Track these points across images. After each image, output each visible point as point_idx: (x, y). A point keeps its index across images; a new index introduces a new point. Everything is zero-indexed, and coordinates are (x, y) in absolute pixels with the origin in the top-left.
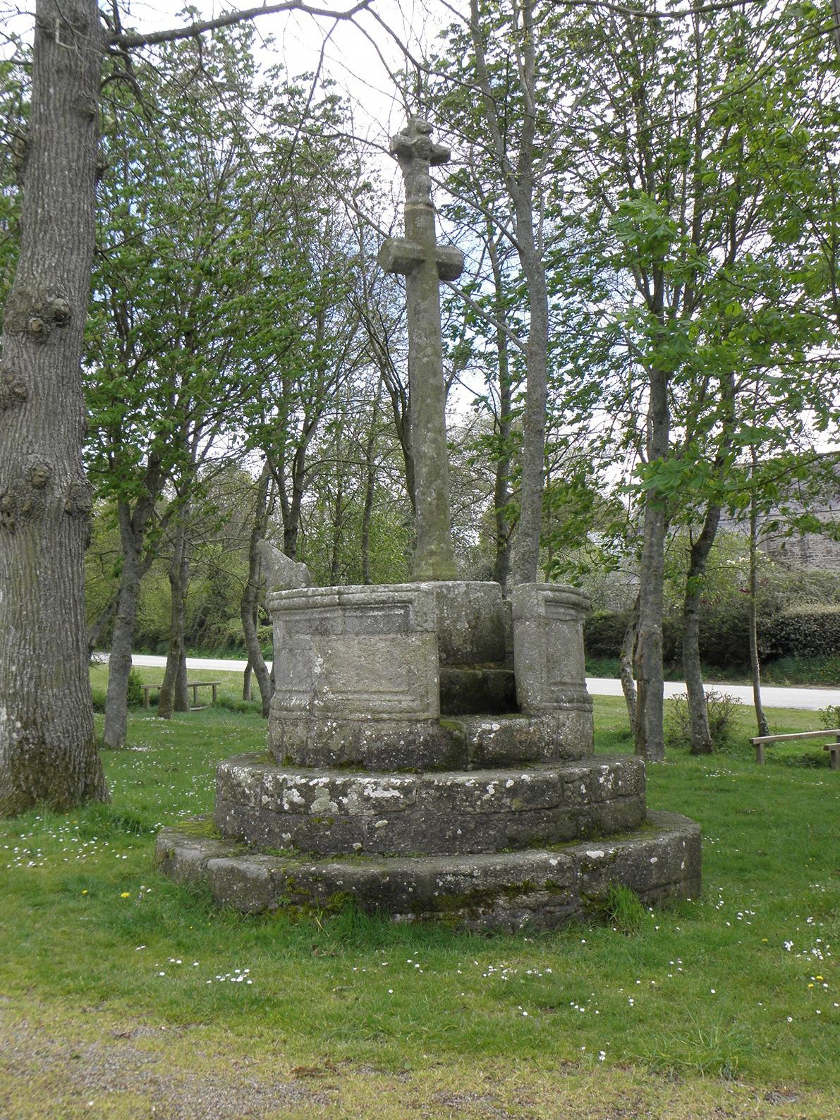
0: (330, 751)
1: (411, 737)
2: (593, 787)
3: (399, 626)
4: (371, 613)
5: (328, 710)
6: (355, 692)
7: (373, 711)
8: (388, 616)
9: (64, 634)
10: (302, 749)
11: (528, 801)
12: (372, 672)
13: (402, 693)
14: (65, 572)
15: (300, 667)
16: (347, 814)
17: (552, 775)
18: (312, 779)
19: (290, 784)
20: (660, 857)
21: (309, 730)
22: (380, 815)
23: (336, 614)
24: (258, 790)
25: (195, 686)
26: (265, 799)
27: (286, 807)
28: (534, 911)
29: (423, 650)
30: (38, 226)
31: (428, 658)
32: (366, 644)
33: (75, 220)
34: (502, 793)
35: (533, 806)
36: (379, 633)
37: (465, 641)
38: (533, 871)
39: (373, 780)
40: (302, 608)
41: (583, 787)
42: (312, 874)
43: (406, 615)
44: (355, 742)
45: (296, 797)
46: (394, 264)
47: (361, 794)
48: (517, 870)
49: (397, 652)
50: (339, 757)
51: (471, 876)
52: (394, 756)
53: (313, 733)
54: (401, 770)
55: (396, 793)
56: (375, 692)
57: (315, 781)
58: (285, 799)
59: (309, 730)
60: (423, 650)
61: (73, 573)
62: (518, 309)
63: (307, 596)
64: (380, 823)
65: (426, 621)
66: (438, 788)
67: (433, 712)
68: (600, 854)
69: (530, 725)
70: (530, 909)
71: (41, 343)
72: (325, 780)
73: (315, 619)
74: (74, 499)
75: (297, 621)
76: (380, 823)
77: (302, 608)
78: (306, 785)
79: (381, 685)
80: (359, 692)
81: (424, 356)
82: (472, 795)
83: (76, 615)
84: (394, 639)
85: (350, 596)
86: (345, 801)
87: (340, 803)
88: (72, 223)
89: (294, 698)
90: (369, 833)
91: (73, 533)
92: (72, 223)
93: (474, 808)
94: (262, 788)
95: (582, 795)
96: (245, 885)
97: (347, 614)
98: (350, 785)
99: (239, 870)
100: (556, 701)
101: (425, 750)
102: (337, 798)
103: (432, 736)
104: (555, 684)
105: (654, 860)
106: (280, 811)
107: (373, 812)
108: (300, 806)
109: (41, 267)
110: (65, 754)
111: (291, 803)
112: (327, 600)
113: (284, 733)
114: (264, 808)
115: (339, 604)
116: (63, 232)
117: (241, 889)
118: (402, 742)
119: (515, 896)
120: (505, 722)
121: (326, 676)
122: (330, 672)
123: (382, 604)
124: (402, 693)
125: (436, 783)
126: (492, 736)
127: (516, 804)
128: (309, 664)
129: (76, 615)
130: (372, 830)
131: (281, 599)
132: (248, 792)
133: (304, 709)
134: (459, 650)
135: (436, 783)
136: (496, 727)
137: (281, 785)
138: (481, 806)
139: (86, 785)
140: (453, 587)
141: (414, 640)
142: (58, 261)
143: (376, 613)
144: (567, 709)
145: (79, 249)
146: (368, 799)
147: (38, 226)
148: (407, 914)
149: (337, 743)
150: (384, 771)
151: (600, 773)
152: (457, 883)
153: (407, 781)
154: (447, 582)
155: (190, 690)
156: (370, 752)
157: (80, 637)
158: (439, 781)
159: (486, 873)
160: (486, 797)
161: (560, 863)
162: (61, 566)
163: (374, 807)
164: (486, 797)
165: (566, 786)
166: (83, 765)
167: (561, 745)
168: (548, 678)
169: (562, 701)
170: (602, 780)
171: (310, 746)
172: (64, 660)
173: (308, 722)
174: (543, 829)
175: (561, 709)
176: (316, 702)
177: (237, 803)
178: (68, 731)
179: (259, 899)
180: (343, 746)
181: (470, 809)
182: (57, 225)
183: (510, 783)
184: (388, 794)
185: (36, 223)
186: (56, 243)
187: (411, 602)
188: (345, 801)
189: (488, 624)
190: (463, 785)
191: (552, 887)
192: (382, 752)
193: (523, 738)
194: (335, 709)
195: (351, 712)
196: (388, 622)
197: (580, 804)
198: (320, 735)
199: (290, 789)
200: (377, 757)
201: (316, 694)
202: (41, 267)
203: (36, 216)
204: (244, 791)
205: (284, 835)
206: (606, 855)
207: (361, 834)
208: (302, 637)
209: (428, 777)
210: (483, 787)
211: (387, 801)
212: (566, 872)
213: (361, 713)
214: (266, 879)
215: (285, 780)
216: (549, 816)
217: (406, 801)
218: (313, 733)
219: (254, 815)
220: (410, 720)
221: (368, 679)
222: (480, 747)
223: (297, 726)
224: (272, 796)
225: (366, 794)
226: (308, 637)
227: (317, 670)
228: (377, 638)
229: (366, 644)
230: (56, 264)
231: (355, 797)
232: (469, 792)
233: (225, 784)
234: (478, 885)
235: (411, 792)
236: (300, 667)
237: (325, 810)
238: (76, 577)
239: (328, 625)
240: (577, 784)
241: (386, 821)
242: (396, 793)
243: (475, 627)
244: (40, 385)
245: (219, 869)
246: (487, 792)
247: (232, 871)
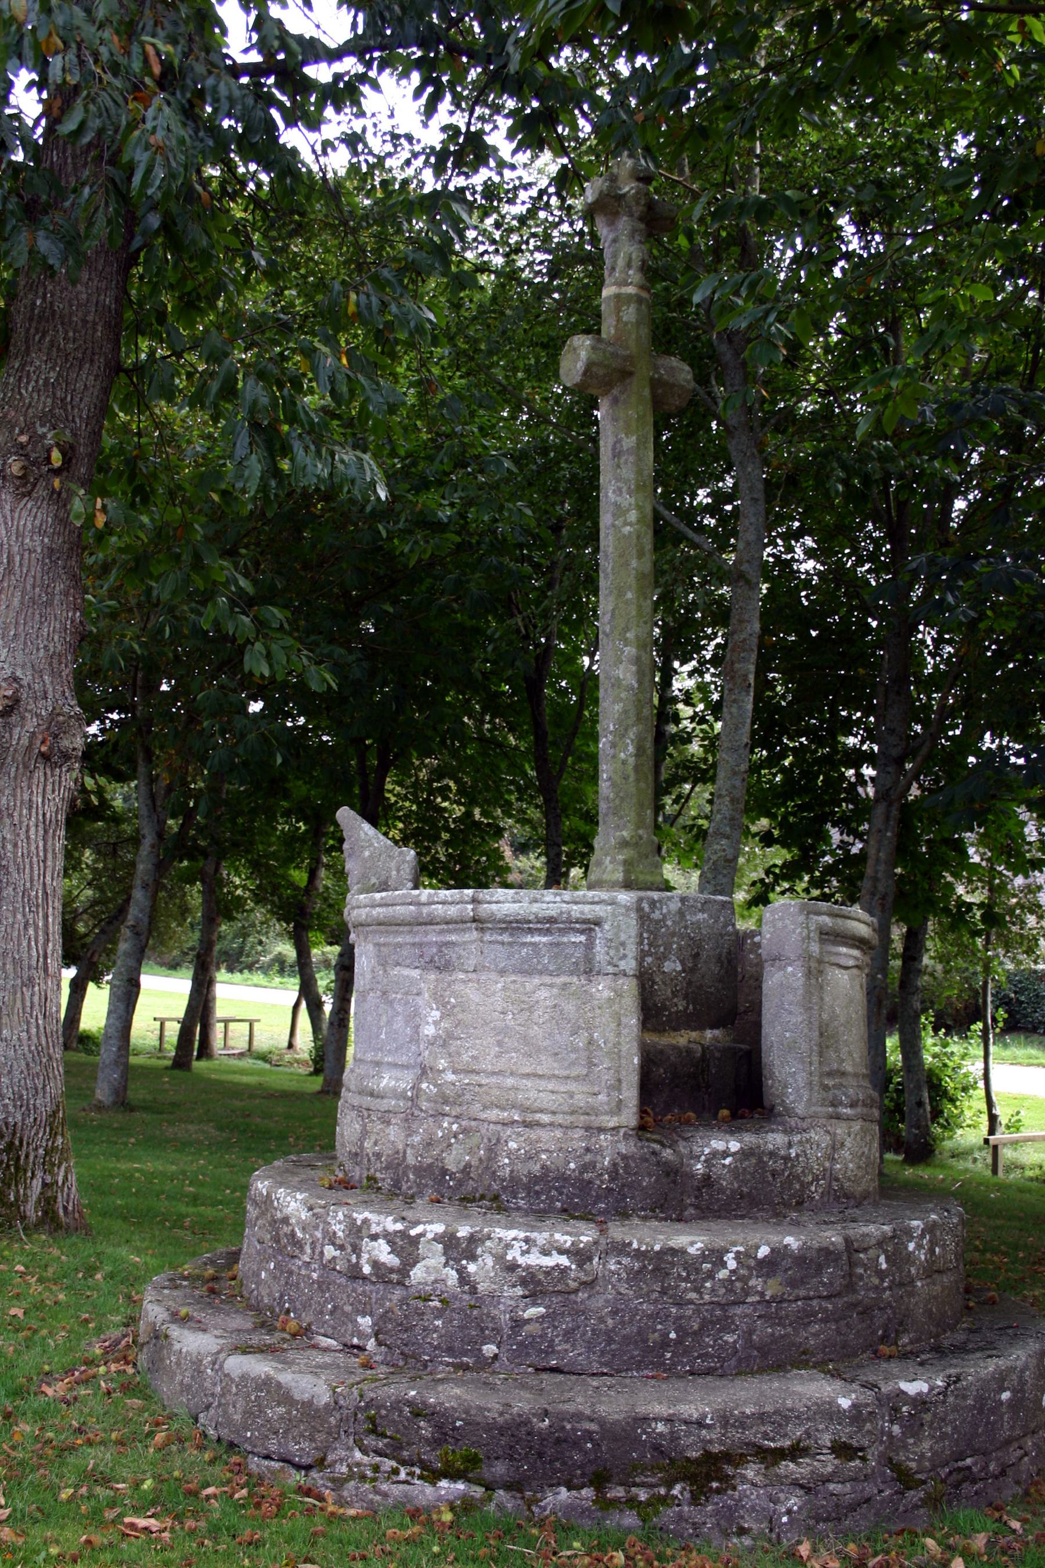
0: (444, 1172)
1: (588, 1157)
2: (899, 1258)
3: (576, 964)
4: (529, 939)
5: (446, 1102)
6: (494, 1073)
7: (525, 1109)
8: (558, 944)
9: (25, 944)
10: (396, 1165)
11: (793, 1284)
12: (525, 1039)
13: (577, 1078)
14: (33, 848)
15: (399, 1023)
16: (473, 1290)
17: (833, 1237)
18: (417, 1223)
19: (375, 1229)
20: (1014, 1391)
21: (410, 1132)
22: (533, 1296)
23: (467, 937)
24: (319, 1234)
25: (226, 1022)
26: (330, 1251)
27: (367, 1269)
28: (807, 1490)
29: (616, 1007)
30: (34, 325)
31: (624, 1020)
32: (515, 992)
33: (90, 318)
34: (749, 1268)
35: (802, 1293)
36: (541, 973)
37: (675, 994)
38: (808, 1419)
39: (522, 1235)
40: (409, 924)
41: (882, 1259)
42: (410, 1403)
43: (590, 945)
44: (489, 1159)
45: (383, 1252)
46: (585, 373)
47: (500, 1258)
48: (781, 1418)
49: (569, 1007)
50: (460, 1183)
51: (700, 1424)
52: (556, 1189)
53: (417, 1139)
54: (569, 1213)
55: (564, 1261)
56: (527, 1076)
57: (419, 1229)
58: (365, 1256)
59: (410, 1132)
60: (616, 1007)
61: (45, 850)
62: (297, 867)
63: (419, 904)
64: (533, 1312)
65: (625, 956)
66: (638, 1254)
67: (629, 1117)
68: (924, 1387)
69: (790, 1145)
70: (802, 1487)
71: (24, 495)
72: (439, 1228)
73: (430, 944)
74: (56, 736)
75: (400, 945)
76: (533, 1312)
77: (409, 924)
78: (403, 1234)
79: (540, 1063)
80: (500, 1073)
81: (626, 524)
82: (698, 1271)
83: (46, 917)
84: (565, 986)
85: (494, 907)
86: (472, 1268)
87: (461, 1271)
88: (85, 322)
89: (387, 1076)
90: (512, 1328)
91: (49, 787)
92: (85, 322)
93: (700, 1293)
94: (325, 1233)
95: (881, 1274)
96: (289, 1412)
97: (487, 937)
98: (482, 1241)
99: (279, 1385)
100: (833, 1105)
101: (612, 1179)
102: (458, 1261)
103: (624, 1157)
104: (830, 1074)
105: (1006, 1396)
106: (354, 1274)
107: (519, 1291)
108: (392, 1270)
109: (33, 383)
110: (14, 1133)
111: (376, 1264)
112: (452, 911)
113: (365, 1133)
114: (329, 1267)
115: (474, 920)
116: (71, 334)
117: (281, 1418)
118: (572, 1166)
119: (775, 1463)
120: (750, 1139)
121: (444, 1041)
122: (450, 1036)
123: (548, 924)
124: (577, 1078)
125: (635, 1245)
126: (728, 1161)
127: (772, 1288)
128: (414, 1018)
129: (46, 917)
130: (518, 1323)
131: (373, 906)
132: (299, 1234)
133: (403, 1096)
134: (665, 1008)
135: (635, 1245)
136: (734, 1146)
137: (359, 1229)
138: (713, 1290)
139: (45, 1185)
140: (660, 901)
141: (602, 989)
142: (59, 374)
143: (537, 939)
144: (848, 1119)
145: (92, 361)
146: (513, 1267)
147: (34, 325)
148: (579, 1488)
149: (454, 1159)
150: (540, 1215)
151: (908, 1232)
152: (674, 1437)
153: (584, 1239)
154: (650, 893)
155: (219, 1027)
156: (514, 1179)
157: (49, 952)
158: (640, 1243)
159: (724, 1420)
160: (723, 1274)
161: (854, 1406)
162: (28, 838)
163: (523, 1282)
164: (723, 1274)
165: (856, 1256)
166: (41, 1151)
167: (837, 1180)
168: (820, 1063)
169: (841, 1103)
170: (911, 1246)
171: (411, 1160)
172: (23, 984)
173: (409, 1120)
174: (816, 1335)
175: (838, 1117)
176: (424, 1086)
177: (280, 1251)
178: (21, 1097)
179: (312, 1439)
180: (468, 1165)
181: (693, 1295)
182: (62, 324)
183: (763, 1251)
184: (549, 1262)
185: (31, 319)
186: (59, 349)
187: (598, 923)
188: (472, 1268)
189: (715, 969)
190: (683, 1252)
191: (842, 1450)
192: (535, 1180)
193: (779, 1165)
194: (455, 1100)
195: (485, 1108)
196: (556, 956)
197: (876, 1288)
198: (429, 1144)
199: (374, 1237)
200: (528, 1189)
201: (424, 1072)
202: (33, 383)
203: (33, 310)
204: (293, 1232)
205: (360, 1319)
206: (931, 1389)
207: (497, 1330)
208: (406, 972)
209: (618, 1232)
210: (717, 1257)
211: (547, 1273)
212: (865, 1421)
213: (503, 1109)
214: (327, 1405)
215: (365, 1221)
216: (826, 1310)
217: (582, 1275)
218: (417, 1139)
219: (309, 1277)
220: (587, 1128)
221: (516, 1050)
222: (707, 1180)
223: (388, 1123)
224: (341, 1248)
225: (509, 1257)
226: (415, 973)
227: (429, 1030)
228: (537, 981)
229: (515, 992)
230: (56, 380)
231: (490, 1261)
232: (692, 1265)
233: (263, 1214)
234: (710, 1441)
235: (590, 1259)
236: (399, 1023)
237: (436, 1281)
238: (50, 856)
239: (451, 954)
240: (872, 1253)
241: (542, 1310)
242: (564, 1261)
243: (693, 970)
244: (17, 558)
245: (244, 1377)
246: (724, 1265)
247: (267, 1384)
